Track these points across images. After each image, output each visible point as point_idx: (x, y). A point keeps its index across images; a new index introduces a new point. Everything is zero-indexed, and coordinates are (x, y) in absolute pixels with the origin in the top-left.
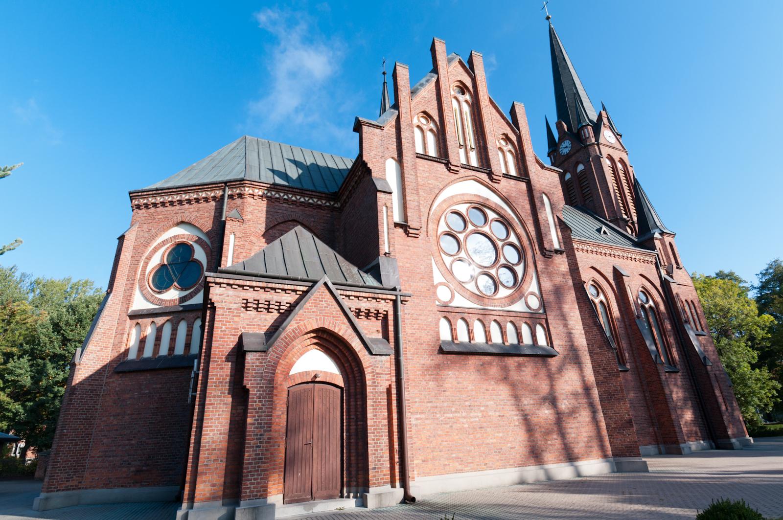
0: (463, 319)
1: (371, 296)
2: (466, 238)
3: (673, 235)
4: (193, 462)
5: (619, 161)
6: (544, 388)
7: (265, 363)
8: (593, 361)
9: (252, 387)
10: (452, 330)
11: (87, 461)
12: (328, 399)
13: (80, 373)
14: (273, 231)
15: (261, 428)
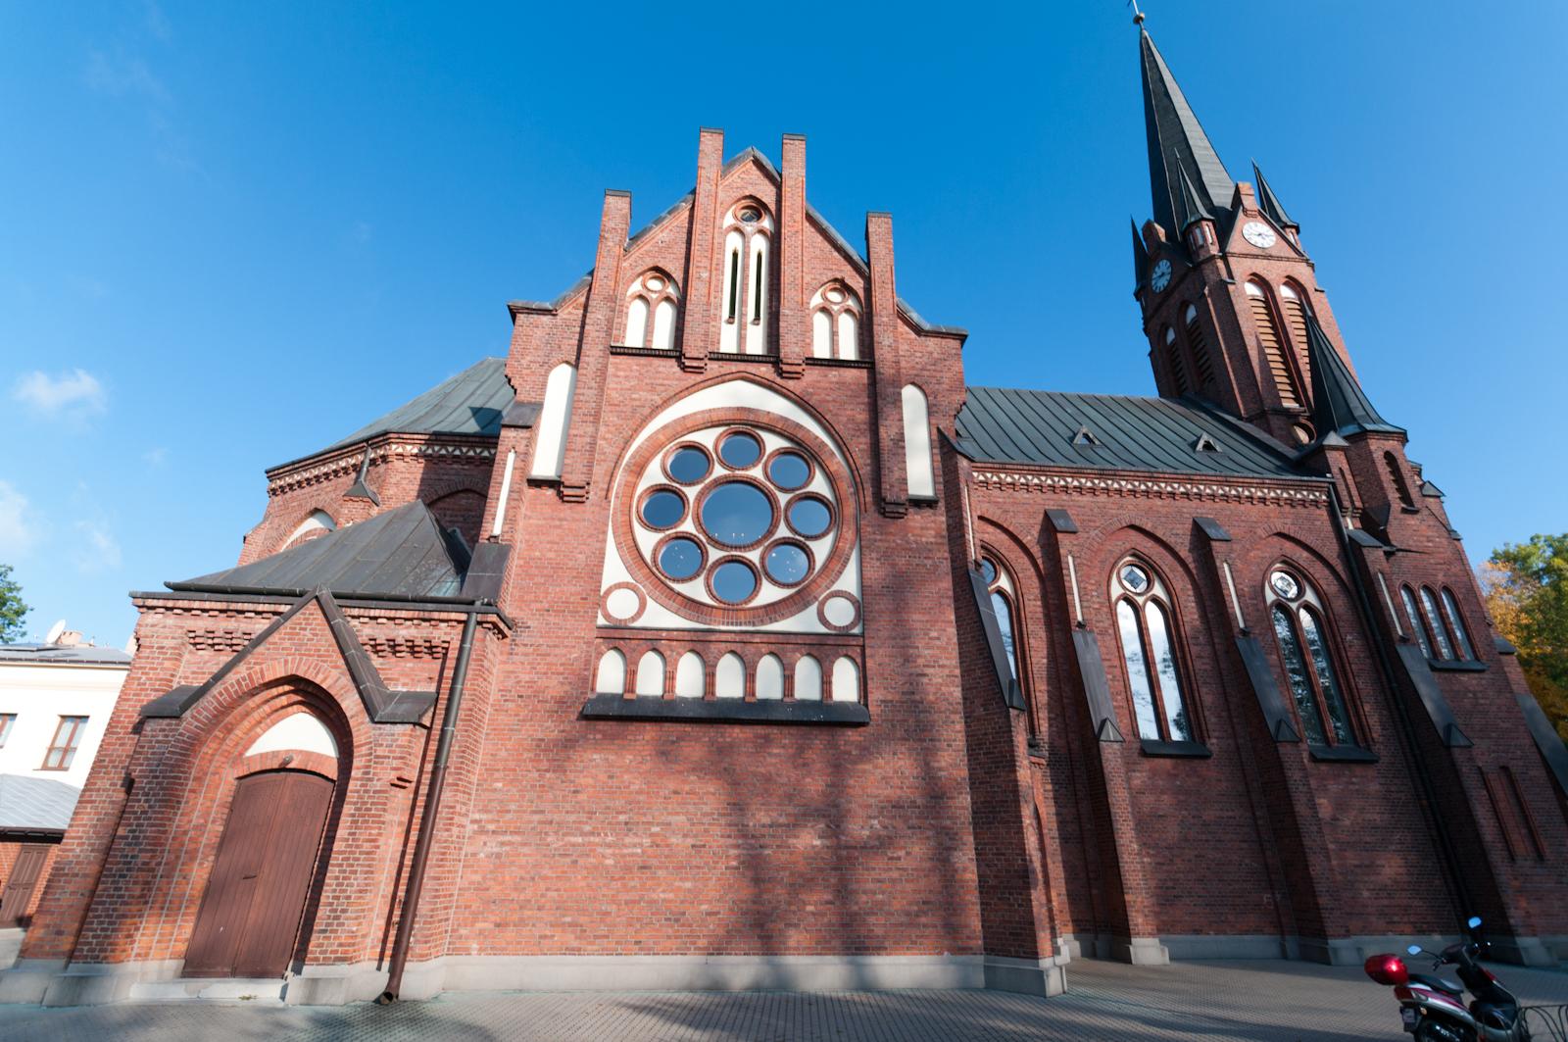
6: (815, 785)
9: (140, 777)
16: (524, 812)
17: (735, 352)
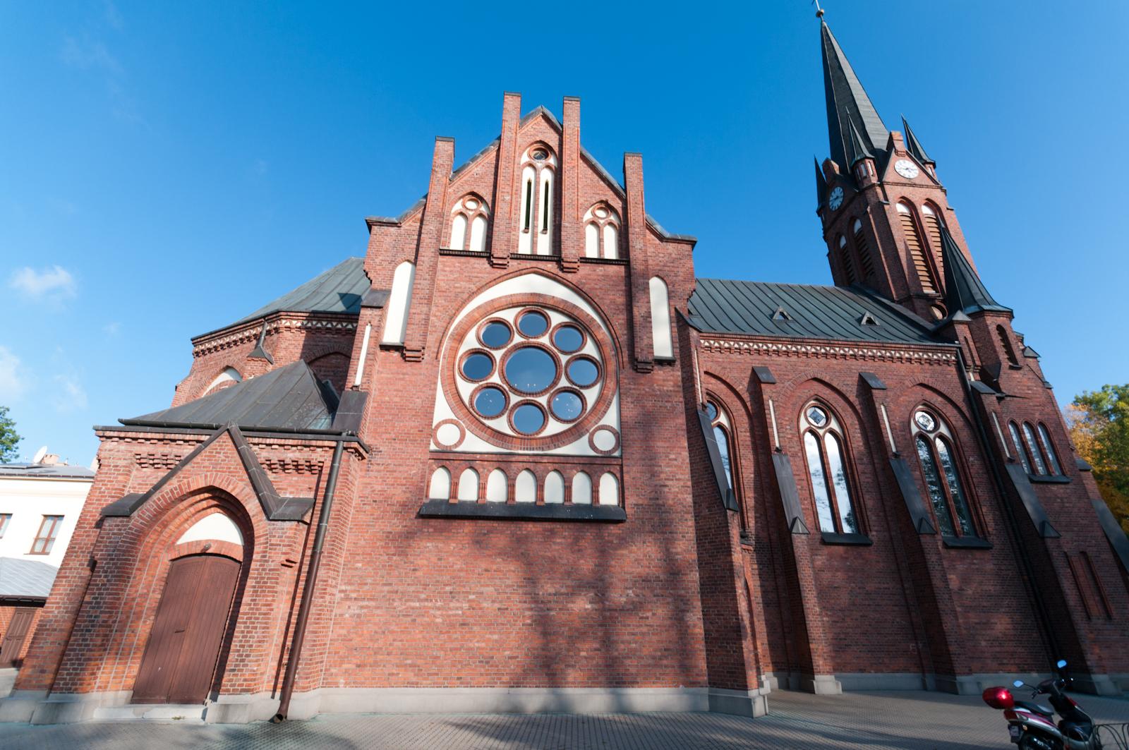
6: (587, 565)
9: (101, 559)
16: (378, 584)
17: (529, 253)
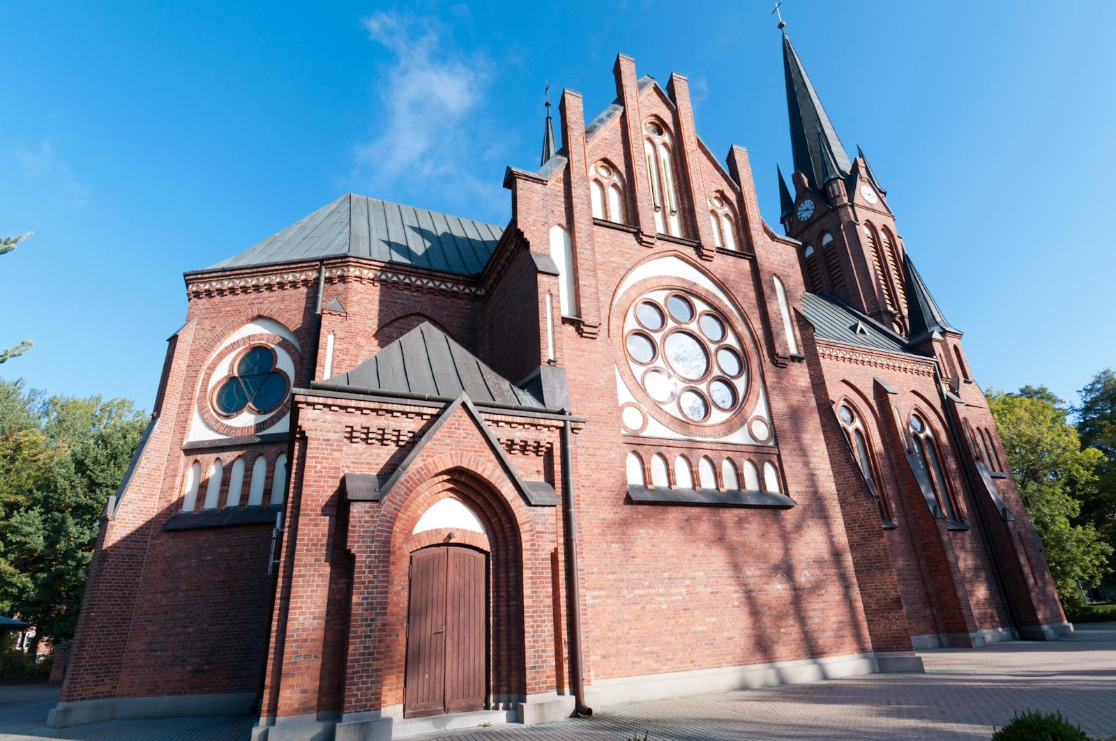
0: (660, 454)
1: (528, 422)
2: (664, 339)
3: (959, 335)
4: (275, 659)
5: (882, 230)
6: (776, 553)
7: (378, 517)
8: (845, 515)
9: (360, 552)
10: (644, 470)
11: (124, 657)
12: (467, 569)
13: (114, 531)
14: (389, 329)
15: (371, 609)
